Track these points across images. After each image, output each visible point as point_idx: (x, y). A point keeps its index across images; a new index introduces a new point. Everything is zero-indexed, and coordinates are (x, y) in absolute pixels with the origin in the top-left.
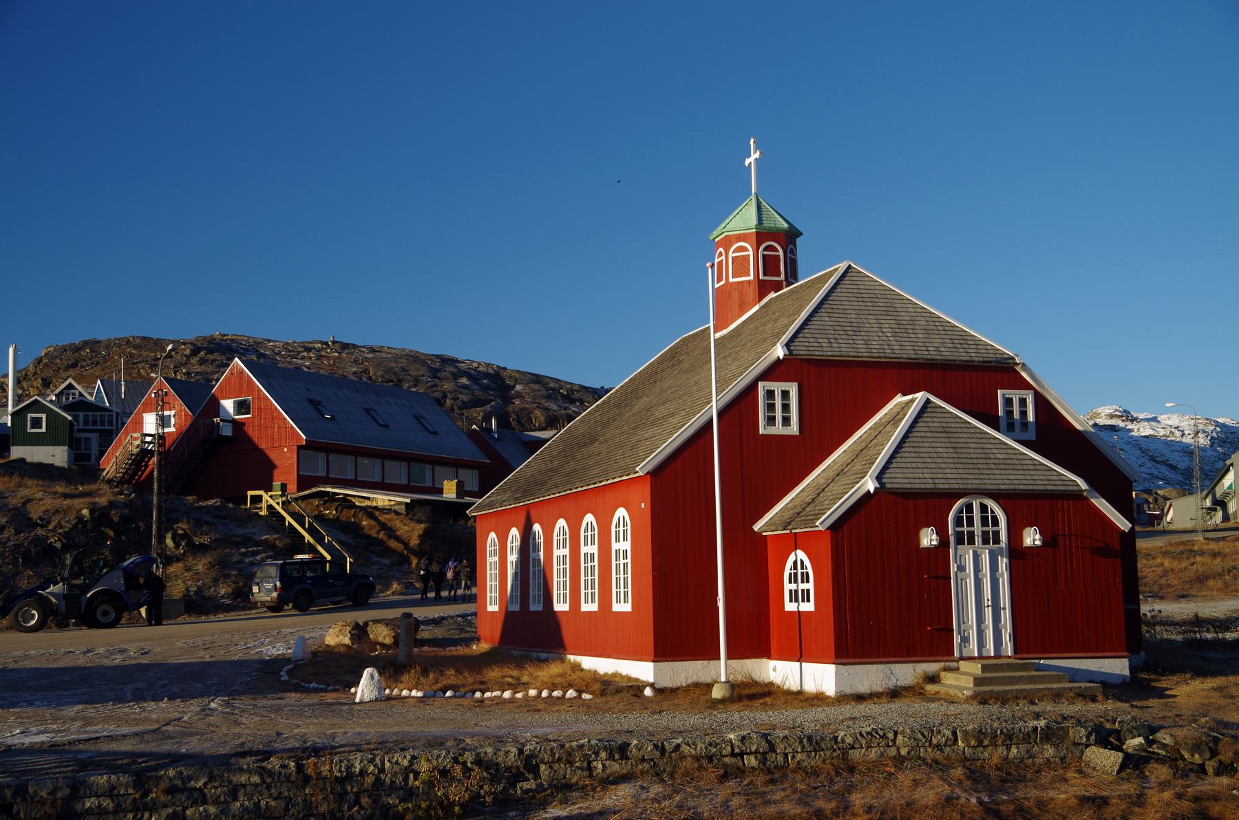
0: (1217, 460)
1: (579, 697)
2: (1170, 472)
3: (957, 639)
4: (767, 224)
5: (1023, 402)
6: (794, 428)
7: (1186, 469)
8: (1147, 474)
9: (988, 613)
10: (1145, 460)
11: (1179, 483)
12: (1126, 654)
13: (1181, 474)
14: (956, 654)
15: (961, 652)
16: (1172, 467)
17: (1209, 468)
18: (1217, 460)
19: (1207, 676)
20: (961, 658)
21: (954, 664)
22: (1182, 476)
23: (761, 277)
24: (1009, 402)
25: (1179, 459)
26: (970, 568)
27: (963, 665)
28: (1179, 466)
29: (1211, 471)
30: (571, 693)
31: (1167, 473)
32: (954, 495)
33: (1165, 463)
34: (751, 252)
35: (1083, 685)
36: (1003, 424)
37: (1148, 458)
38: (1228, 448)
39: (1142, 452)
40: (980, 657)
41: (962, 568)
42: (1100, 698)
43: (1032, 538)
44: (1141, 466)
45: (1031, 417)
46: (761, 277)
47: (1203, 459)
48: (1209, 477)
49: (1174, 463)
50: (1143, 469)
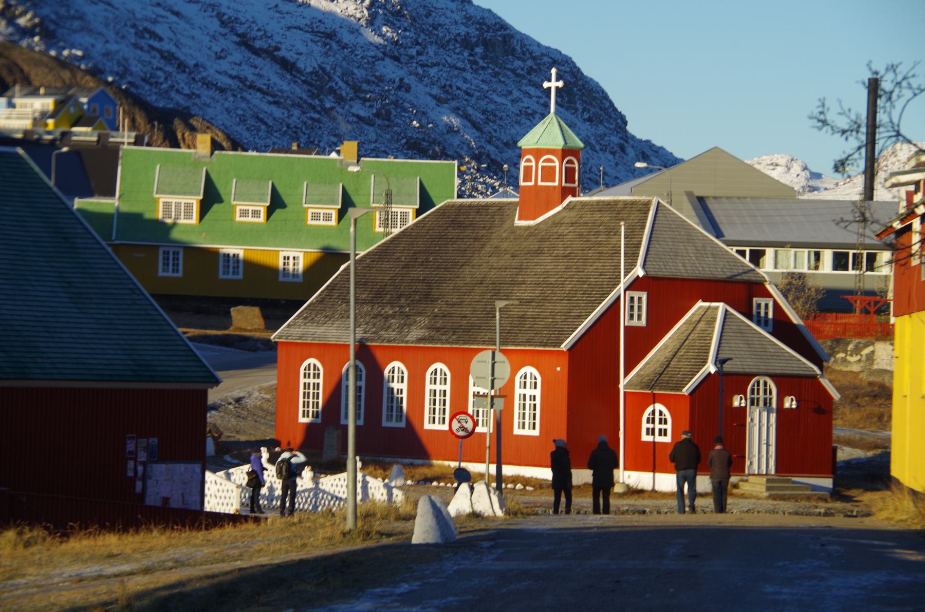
0: (380, 55)
1: (525, 488)
2: (282, 77)
3: (747, 463)
4: (571, 144)
5: (767, 306)
6: (643, 322)
7: (314, 72)
8: (231, 77)
9: (764, 447)
10: (228, 42)
11: (299, 106)
12: (831, 476)
13: (304, 82)
14: (747, 472)
15: (749, 470)
16: (287, 66)
17: (363, 72)
18: (380, 55)
19: (184, 526)
20: (749, 475)
21: (745, 478)
22: (305, 87)
23: (564, 184)
24: (759, 306)
25: (303, 49)
26: (756, 421)
27: (751, 478)
28: (301, 65)
29: (368, 82)
30: (519, 486)
31: (275, 79)
32: (754, 375)
33: (271, 54)
34: (557, 164)
35: (821, 493)
36: (755, 318)
37: (235, 39)
38: (405, 30)
39: (223, 24)
40: (767, 474)
41: (752, 420)
42: (829, 500)
43: (790, 403)
44: (220, 58)
45: (770, 316)
46: (564, 184)
47: (352, 52)
48: (362, 95)
49: (291, 56)
50: (224, 65)
